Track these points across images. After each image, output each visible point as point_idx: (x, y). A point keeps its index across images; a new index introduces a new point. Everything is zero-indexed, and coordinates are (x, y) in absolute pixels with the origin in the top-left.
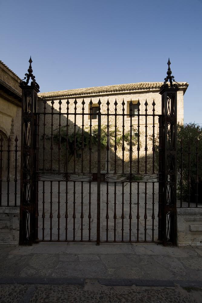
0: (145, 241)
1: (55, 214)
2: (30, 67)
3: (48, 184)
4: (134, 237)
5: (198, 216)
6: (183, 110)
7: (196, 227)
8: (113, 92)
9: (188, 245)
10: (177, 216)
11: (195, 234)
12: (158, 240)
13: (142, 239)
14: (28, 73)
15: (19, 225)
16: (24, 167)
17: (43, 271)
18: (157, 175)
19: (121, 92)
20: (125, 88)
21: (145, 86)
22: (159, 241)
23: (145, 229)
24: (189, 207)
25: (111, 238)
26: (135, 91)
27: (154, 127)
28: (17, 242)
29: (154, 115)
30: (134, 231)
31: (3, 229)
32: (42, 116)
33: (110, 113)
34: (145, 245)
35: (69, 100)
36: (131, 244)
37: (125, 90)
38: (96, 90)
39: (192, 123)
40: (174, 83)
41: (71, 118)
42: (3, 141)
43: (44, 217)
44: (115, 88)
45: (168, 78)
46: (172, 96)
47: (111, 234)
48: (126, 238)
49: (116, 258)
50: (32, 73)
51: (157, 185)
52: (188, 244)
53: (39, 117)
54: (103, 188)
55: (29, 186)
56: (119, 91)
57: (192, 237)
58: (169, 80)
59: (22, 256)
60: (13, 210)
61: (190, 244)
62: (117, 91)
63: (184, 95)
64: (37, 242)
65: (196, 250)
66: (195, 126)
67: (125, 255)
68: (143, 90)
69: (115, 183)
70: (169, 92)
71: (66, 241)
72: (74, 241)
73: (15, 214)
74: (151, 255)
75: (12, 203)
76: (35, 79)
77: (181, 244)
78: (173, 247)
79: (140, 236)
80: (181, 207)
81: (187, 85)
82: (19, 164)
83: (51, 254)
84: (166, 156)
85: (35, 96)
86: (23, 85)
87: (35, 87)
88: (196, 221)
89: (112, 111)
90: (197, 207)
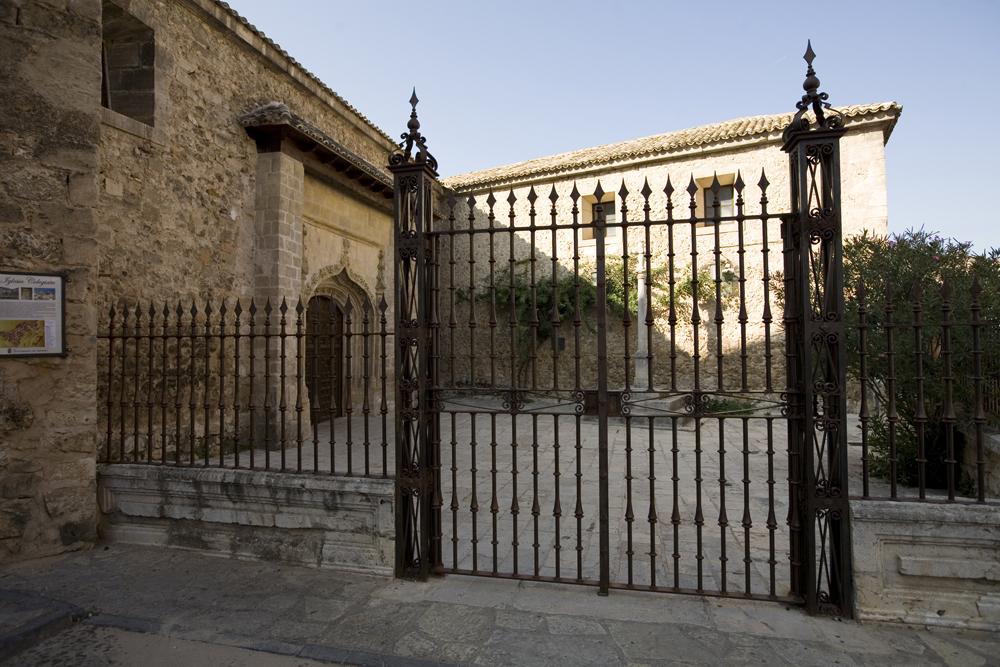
0: (748, 595)
1: (484, 504)
2: (414, 116)
3: (463, 421)
4: (714, 582)
5: (929, 527)
6: (885, 193)
7: (919, 562)
8: (652, 157)
9: (892, 617)
10: (853, 525)
11: (918, 587)
12: (790, 594)
13: (738, 587)
14: (408, 132)
15: (392, 526)
16: (403, 374)
17: (453, 648)
18: (781, 397)
19: (676, 154)
20: (689, 140)
21: (753, 128)
22: (791, 599)
23: (748, 560)
24: (893, 497)
25: (642, 577)
26: (719, 146)
27: (765, 251)
28: (390, 570)
29: (764, 217)
30: (712, 561)
31: (357, 532)
32: (700, 214)
33: (676, 216)
34: (747, 606)
35: (535, 188)
36: (704, 601)
37: (687, 147)
38: (602, 154)
39: (915, 232)
40: (827, 114)
41: (543, 241)
42: (353, 310)
43: (497, 511)
44: (657, 145)
45: (806, 100)
46: (823, 154)
47: (642, 568)
48: (688, 581)
49: (653, 633)
50: (418, 131)
51: (781, 429)
52: (894, 615)
53: (437, 242)
54: (616, 435)
55: (415, 423)
56: (671, 150)
57: (905, 594)
58: (810, 106)
59: (401, 605)
60: (380, 486)
61: (902, 617)
62: (663, 151)
63: (885, 142)
64: (440, 574)
65: (923, 637)
66: (923, 240)
67: (681, 629)
68: (744, 142)
69: (651, 418)
70: (812, 143)
71: (515, 575)
72: (536, 577)
73: (384, 495)
74: (764, 638)
75: (376, 470)
76: (425, 144)
77: (867, 613)
78: (840, 620)
79: (729, 577)
80: (866, 496)
81: (895, 111)
82: (390, 368)
83: (474, 607)
84: (807, 338)
85: (425, 188)
86: (398, 163)
87: (427, 164)
88: (921, 543)
89: (658, 212)
90: (922, 499)
